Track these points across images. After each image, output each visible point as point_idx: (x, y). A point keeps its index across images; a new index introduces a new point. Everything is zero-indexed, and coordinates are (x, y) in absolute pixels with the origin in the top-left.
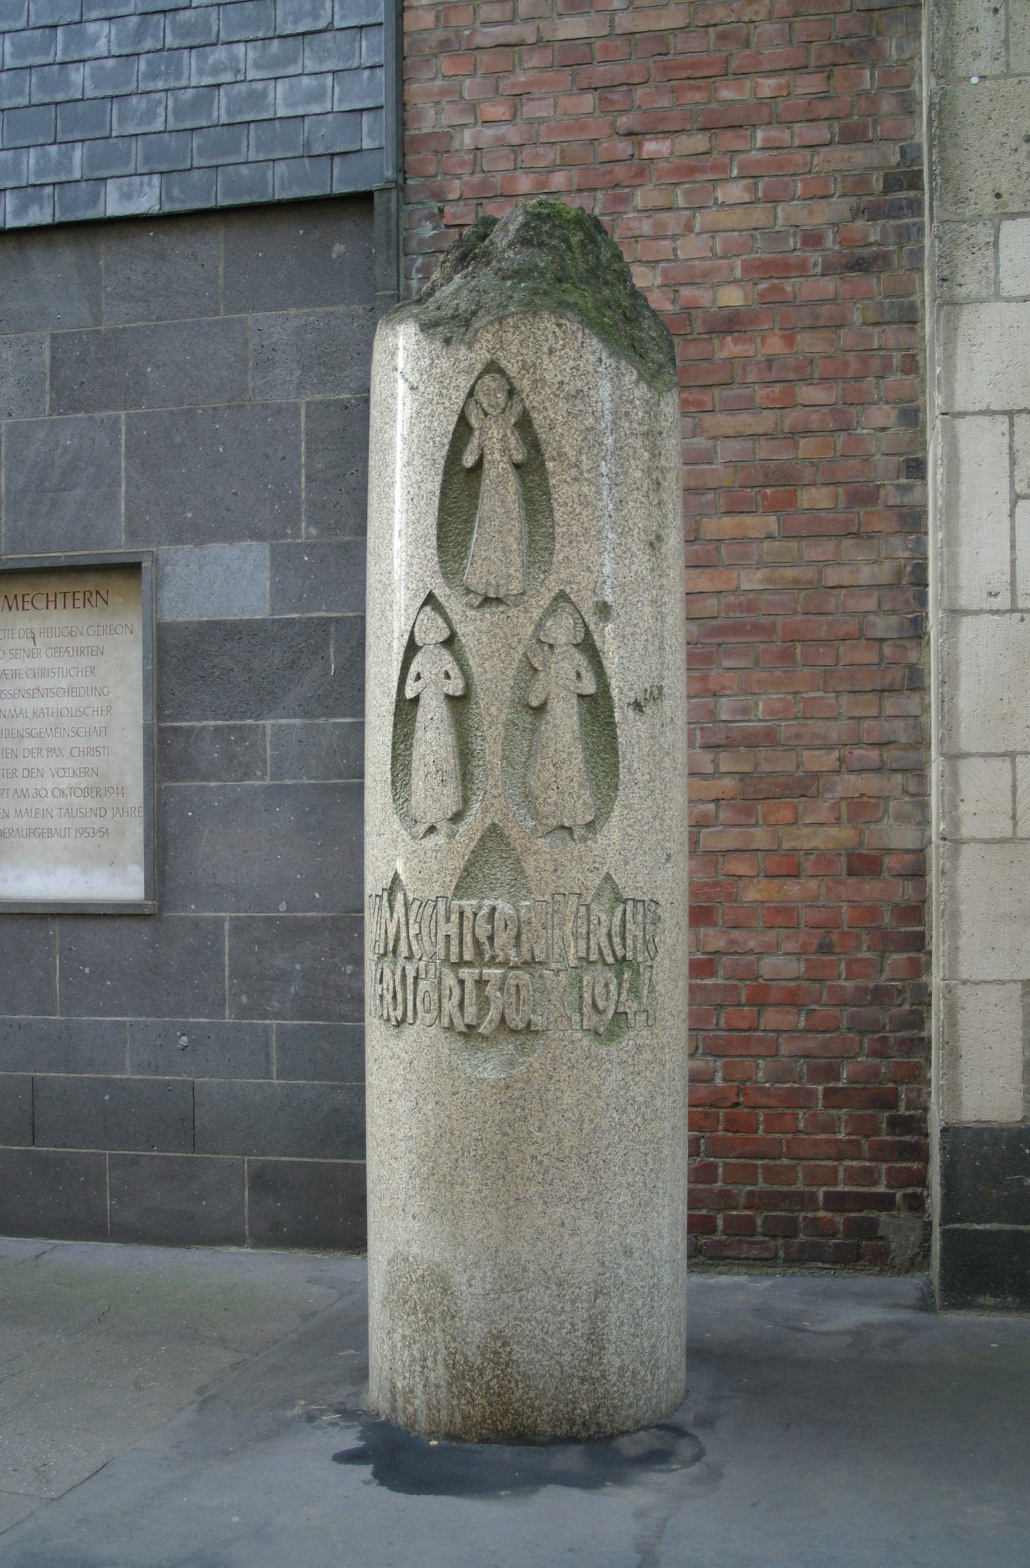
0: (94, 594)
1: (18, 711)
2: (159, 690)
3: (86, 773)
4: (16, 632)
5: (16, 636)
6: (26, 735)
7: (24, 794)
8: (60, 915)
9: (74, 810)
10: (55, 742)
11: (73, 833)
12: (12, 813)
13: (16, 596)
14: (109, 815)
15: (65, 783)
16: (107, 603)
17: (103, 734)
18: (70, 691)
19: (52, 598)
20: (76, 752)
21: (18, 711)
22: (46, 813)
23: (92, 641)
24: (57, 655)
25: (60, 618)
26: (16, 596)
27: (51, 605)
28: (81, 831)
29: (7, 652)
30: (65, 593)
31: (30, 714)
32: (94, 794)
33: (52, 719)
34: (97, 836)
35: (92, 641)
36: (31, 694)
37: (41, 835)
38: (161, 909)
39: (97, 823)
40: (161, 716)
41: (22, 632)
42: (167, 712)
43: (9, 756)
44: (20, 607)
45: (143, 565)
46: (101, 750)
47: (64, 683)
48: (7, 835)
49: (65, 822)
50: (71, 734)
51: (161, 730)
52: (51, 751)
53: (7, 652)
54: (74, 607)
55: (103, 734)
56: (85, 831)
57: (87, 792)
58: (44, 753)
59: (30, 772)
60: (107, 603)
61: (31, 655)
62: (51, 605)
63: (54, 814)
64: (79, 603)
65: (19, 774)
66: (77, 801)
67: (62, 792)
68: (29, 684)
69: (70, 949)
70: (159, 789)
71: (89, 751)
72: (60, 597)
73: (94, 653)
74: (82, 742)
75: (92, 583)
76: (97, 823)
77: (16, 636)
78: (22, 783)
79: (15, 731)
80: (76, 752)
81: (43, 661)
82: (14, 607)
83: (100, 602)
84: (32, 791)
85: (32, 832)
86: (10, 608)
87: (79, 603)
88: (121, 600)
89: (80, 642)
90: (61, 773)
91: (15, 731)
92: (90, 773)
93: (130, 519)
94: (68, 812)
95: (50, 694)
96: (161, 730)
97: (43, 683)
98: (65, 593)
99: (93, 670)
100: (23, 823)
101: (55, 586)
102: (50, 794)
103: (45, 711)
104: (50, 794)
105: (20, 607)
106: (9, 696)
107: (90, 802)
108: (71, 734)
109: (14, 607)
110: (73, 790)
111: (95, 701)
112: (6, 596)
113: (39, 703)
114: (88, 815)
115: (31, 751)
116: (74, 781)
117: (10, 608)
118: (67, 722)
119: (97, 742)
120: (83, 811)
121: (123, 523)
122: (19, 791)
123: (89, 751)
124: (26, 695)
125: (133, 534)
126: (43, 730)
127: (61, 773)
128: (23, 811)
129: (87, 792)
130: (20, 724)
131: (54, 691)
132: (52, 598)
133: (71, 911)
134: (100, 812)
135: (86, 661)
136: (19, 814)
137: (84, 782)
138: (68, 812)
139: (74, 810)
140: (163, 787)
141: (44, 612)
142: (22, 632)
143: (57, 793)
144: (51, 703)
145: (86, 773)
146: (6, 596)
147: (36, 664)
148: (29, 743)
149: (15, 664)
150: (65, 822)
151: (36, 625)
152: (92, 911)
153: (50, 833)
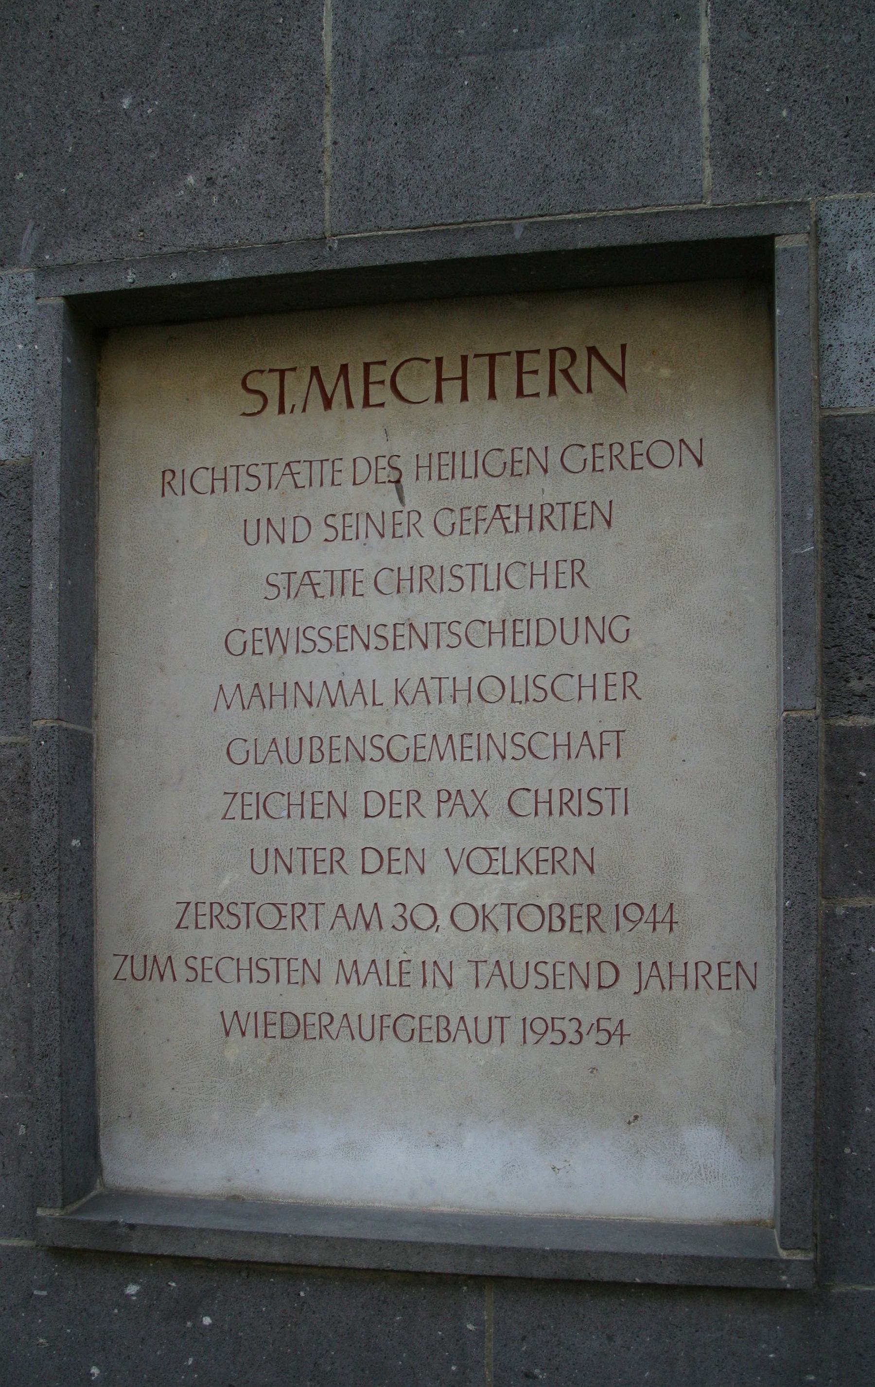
0: (582, 356)
1: (350, 686)
2: (831, 619)
3: (555, 864)
4: (346, 465)
5: (345, 477)
6: (371, 752)
7: (368, 919)
8: (499, 1281)
9: (519, 969)
10: (465, 775)
11: (514, 1029)
12: (329, 971)
13: (344, 369)
14: (629, 983)
15: (490, 891)
16: (621, 380)
17: (610, 752)
18: (510, 631)
19: (452, 369)
20: (524, 802)
21: (350, 686)
22: (436, 974)
23: (576, 488)
24: (469, 527)
25: (478, 424)
26: (344, 369)
27: (452, 390)
28: (539, 1027)
29: (317, 522)
30: (492, 357)
31: (385, 694)
32: (581, 924)
33: (452, 710)
34: (589, 1041)
35: (576, 488)
36: (388, 639)
37: (417, 1035)
38: (824, 1270)
39: (591, 1004)
40: (835, 695)
41: (362, 466)
42: (856, 685)
43: (321, 811)
44: (358, 397)
45: (780, 244)
46: (605, 797)
47: (491, 607)
48: (314, 1032)
49: (492, 1000)
50: (511, 751)
51: (837, 740)
52: (449, 798)
53: (317, 522)
54: (520, 393)
55: (610, 752)
56: (550, 1025)
57: (558, 917)
58: (429, 804)
59: (386, 859)
60: (621, 380)
61: (390, 529)
62: (452, 390)
63: (458, 976)
64: (535, 384)
65: (352, 862)
66: (527, 943)
67: (482, 917)
68: (385, 610)
69: (529, 1375)
70: (831, 915)
71: (567, 802)
72: (478, 370)
73: (583, 522)
74: (544, 775)
75: (573, 326)
76: (591, 1004)
77: (345, 477)
78: (356, 888)
79: (340, 743)
80: (524, 802)
81: (426, 548)
82: (340, 397)
83: (601, 379)
84: (390, 914)
85: (387, 1026)
86: (328, 403)
87: (535, 384)
88: (665, 372)
89: (537, 490)
90: (480, 861)
91: (340, 743)
92: (568, 863)
93: (725, 120)
94: (503, 974)
95: (446, 638)
96: (837, 740)
97: (424, 608)
98: (492, 357)
99: (578, 570)
100: (365, 999)
101: (459, 336)
102: (444, 920)
103: (432, 686)
104: (444, 920)
105: (358, 397)
106: (323, 645)
107: (568, 946)
108: (511, 751)
109: (340, 397)
110: (516, 914)
111: (589, 658)
112: (315, 371)
113: (412, 664)
114: (562, 981)
115: (387, 801)
116: (520, 886)
117: (328, 403)
118: (499, 718)
119: (589, 773)
120: (547, 970)
121: (706, 132)
122: (351, 909)
123: (567, 802)
124: (374, 641)
125: (736, 162)
126: (427, 741)
127: (480, 861)
128: (363, 970)
129: (558, 917)
130: (355, 722)
131: (460, 630)
132: (452, 369)
133: (539, 1271)
134: (603, 976)
135: (556, 544)
136: (350, 974)
137: (549, 889)
138: (503, 974)
139: (519, 969)
140: (840, 911)
141: (432, 409)
142: (362, 466)
143: (466, 917)
144: (449, 663)
145: (555, 864)
146: (315, 371)
147: (405, 553)
148: (383, 777)
149: (343, 556)
150: (492, 1000)
151: (406, 446)
152: (607, 1275)
153: (445, 1030)
